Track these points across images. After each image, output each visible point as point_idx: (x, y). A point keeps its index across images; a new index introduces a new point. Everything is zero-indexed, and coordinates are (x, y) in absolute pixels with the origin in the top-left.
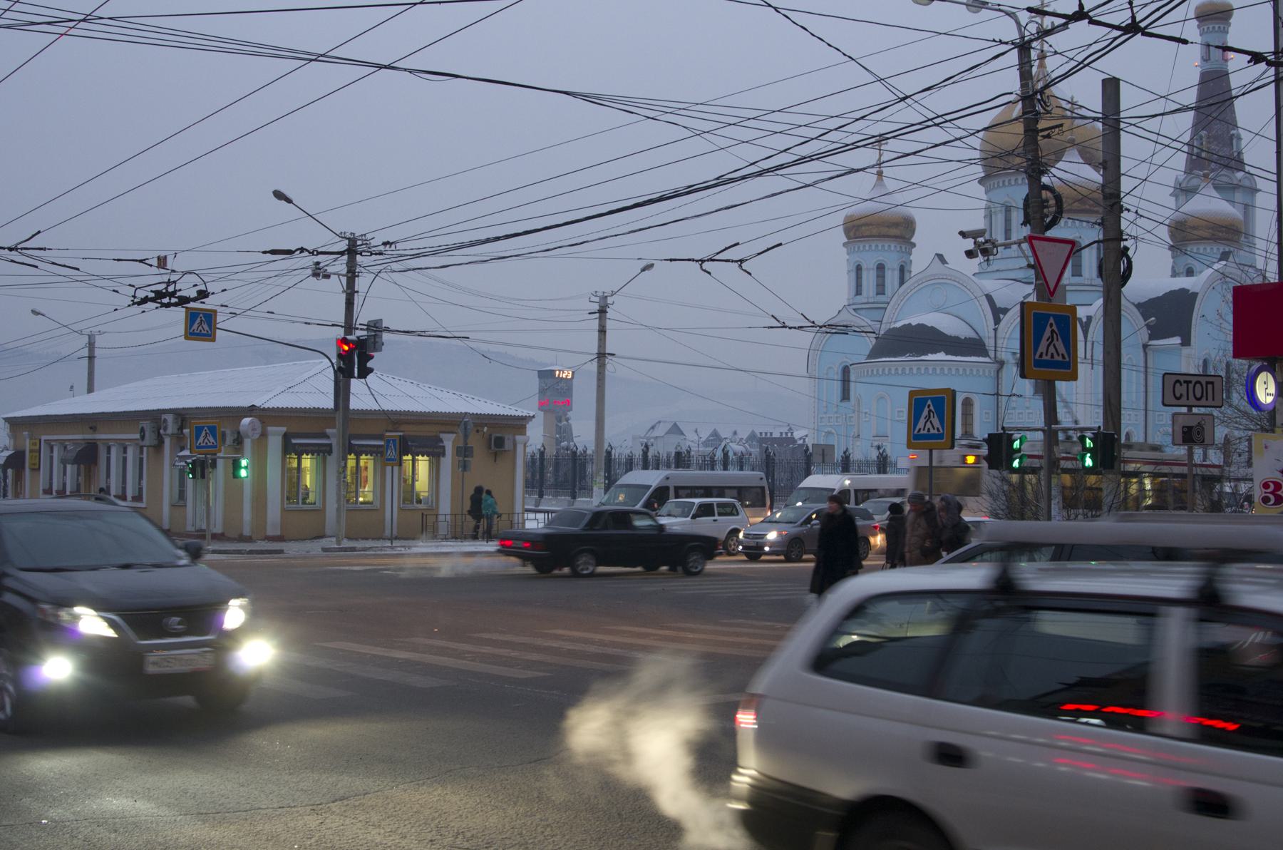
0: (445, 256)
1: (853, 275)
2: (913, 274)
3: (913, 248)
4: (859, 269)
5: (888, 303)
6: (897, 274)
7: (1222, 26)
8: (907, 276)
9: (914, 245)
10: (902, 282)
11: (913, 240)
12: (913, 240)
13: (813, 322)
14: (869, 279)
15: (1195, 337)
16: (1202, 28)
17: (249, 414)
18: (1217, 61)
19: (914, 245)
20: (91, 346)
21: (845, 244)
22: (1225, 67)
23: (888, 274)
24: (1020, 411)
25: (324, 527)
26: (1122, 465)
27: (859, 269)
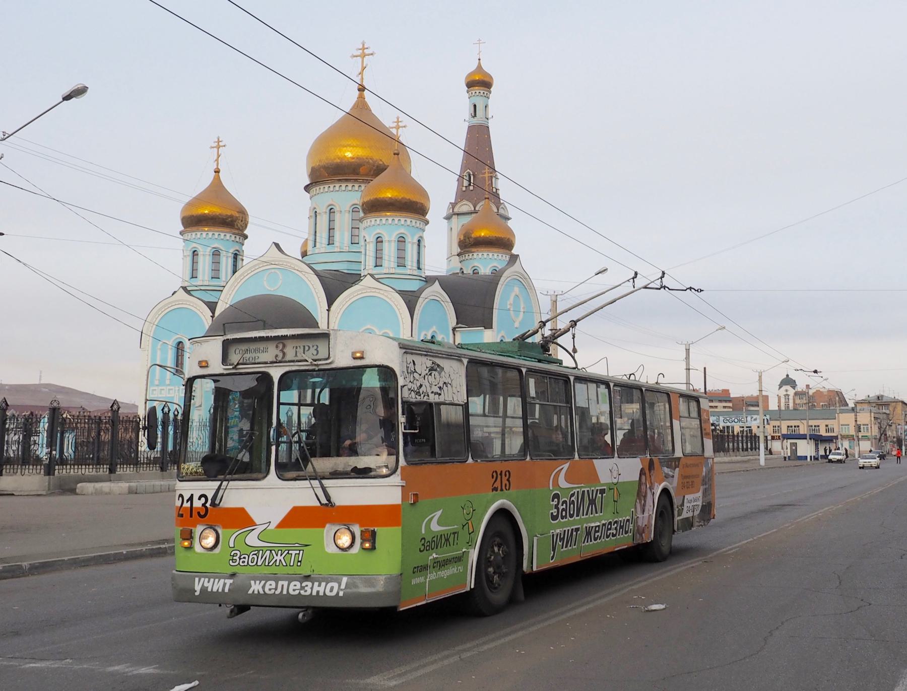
0: (808, 369)
1: (189, 260)
2: (245, 263)
3: (245, 239)
4: (195, 253)
5: (224, 287)
6: (230, 261)
7: (486, 93)
8: (239, 263)
9: (246, 237)
10: (234, 272)
11: (246, 232)
12: (246, 232)
13: (575, 351)
14: (205, 263)
15: (417, 314)
16: (470, 93)
17: (123, 404)
18: (481, 118)
19: (246, 237)
20: (760, 377)
21: (181, 233)
22: (486, 123)
23: (223, 260)
24: (162, 388)
25: (362, 455)
26: (663, 404)
27: (195, 253)
